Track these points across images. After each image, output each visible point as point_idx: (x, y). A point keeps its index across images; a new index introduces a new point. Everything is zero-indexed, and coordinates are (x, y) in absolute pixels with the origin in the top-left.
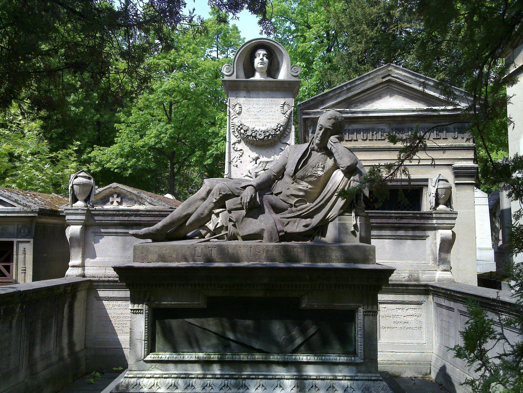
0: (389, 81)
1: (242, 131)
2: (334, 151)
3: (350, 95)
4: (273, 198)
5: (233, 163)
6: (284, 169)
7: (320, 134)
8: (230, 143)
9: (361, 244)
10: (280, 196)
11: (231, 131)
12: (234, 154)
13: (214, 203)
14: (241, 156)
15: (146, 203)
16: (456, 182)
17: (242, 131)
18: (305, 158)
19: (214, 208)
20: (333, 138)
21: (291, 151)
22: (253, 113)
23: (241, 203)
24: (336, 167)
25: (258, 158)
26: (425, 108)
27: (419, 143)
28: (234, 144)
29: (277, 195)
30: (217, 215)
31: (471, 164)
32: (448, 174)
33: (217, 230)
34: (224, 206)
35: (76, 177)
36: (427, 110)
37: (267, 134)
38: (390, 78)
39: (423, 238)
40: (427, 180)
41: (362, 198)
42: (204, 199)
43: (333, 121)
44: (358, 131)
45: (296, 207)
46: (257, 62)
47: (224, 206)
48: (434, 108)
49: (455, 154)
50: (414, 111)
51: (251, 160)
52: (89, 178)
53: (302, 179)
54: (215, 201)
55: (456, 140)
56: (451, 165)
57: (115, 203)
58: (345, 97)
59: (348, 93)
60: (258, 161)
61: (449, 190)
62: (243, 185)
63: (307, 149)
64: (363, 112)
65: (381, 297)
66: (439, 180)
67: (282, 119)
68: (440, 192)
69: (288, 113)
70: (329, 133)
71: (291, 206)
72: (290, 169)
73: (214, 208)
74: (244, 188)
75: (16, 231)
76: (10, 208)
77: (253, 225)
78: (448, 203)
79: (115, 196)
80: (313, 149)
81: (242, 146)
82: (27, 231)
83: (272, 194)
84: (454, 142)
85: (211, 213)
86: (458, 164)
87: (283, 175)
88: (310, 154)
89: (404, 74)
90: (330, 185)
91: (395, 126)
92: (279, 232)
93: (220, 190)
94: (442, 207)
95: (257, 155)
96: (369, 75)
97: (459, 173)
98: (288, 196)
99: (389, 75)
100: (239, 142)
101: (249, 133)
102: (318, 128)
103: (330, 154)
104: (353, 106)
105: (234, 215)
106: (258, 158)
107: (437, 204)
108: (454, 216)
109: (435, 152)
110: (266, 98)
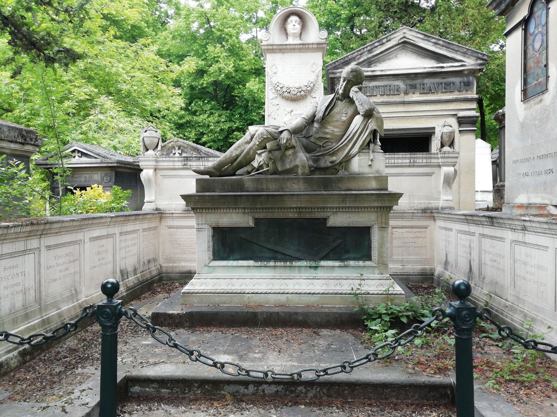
0: (405, 42)
1: (279, 88)
2: (355, 99)
3: (370, 56)
6: (314, 116)
7: (344, 85)
13: (258, 145)
16: (460, 129)
17: (279, 88)
18: (330, 107)
20: (355, 88)
21: (319, 101)
24: (356, 113)
25: (292, 111)
30: (260, 154)
32: (453, 122)
33: (260, 167)
37: (300, 90)
40: (434, 128)
41: (378, 137)
42: (248, 143)
45: (324, 147)
47: (265, 148)
50: (425, 68)
51: (286, 113)
54: (257, 143)
55: (461, 93)
56: (456, 115)
58: (365, 58)
60: (292, 114)
61: (452, 134)
62: (280, 130)
64: (382, 71)
65: (392, 223)
66: (445, 126)
68: (444, 136)
71: (320, 146)
74: (281, 132)
75: (100, 178)
76: (93, 160)
78: (452, 145)
79: (177, 148)
82: (108, 178)
84: (460, 95)
85: (255, 153)
86: (461, 114)
90: (352, 126)
91: (409, 82)
94: (446, 149)
95: (291, 109)
97: (462, 121)
101: (284, 90)
103: (352, 102)
104: (373, 65)
106: (292, 111)
107: (442, 146)
108: (456, 155)
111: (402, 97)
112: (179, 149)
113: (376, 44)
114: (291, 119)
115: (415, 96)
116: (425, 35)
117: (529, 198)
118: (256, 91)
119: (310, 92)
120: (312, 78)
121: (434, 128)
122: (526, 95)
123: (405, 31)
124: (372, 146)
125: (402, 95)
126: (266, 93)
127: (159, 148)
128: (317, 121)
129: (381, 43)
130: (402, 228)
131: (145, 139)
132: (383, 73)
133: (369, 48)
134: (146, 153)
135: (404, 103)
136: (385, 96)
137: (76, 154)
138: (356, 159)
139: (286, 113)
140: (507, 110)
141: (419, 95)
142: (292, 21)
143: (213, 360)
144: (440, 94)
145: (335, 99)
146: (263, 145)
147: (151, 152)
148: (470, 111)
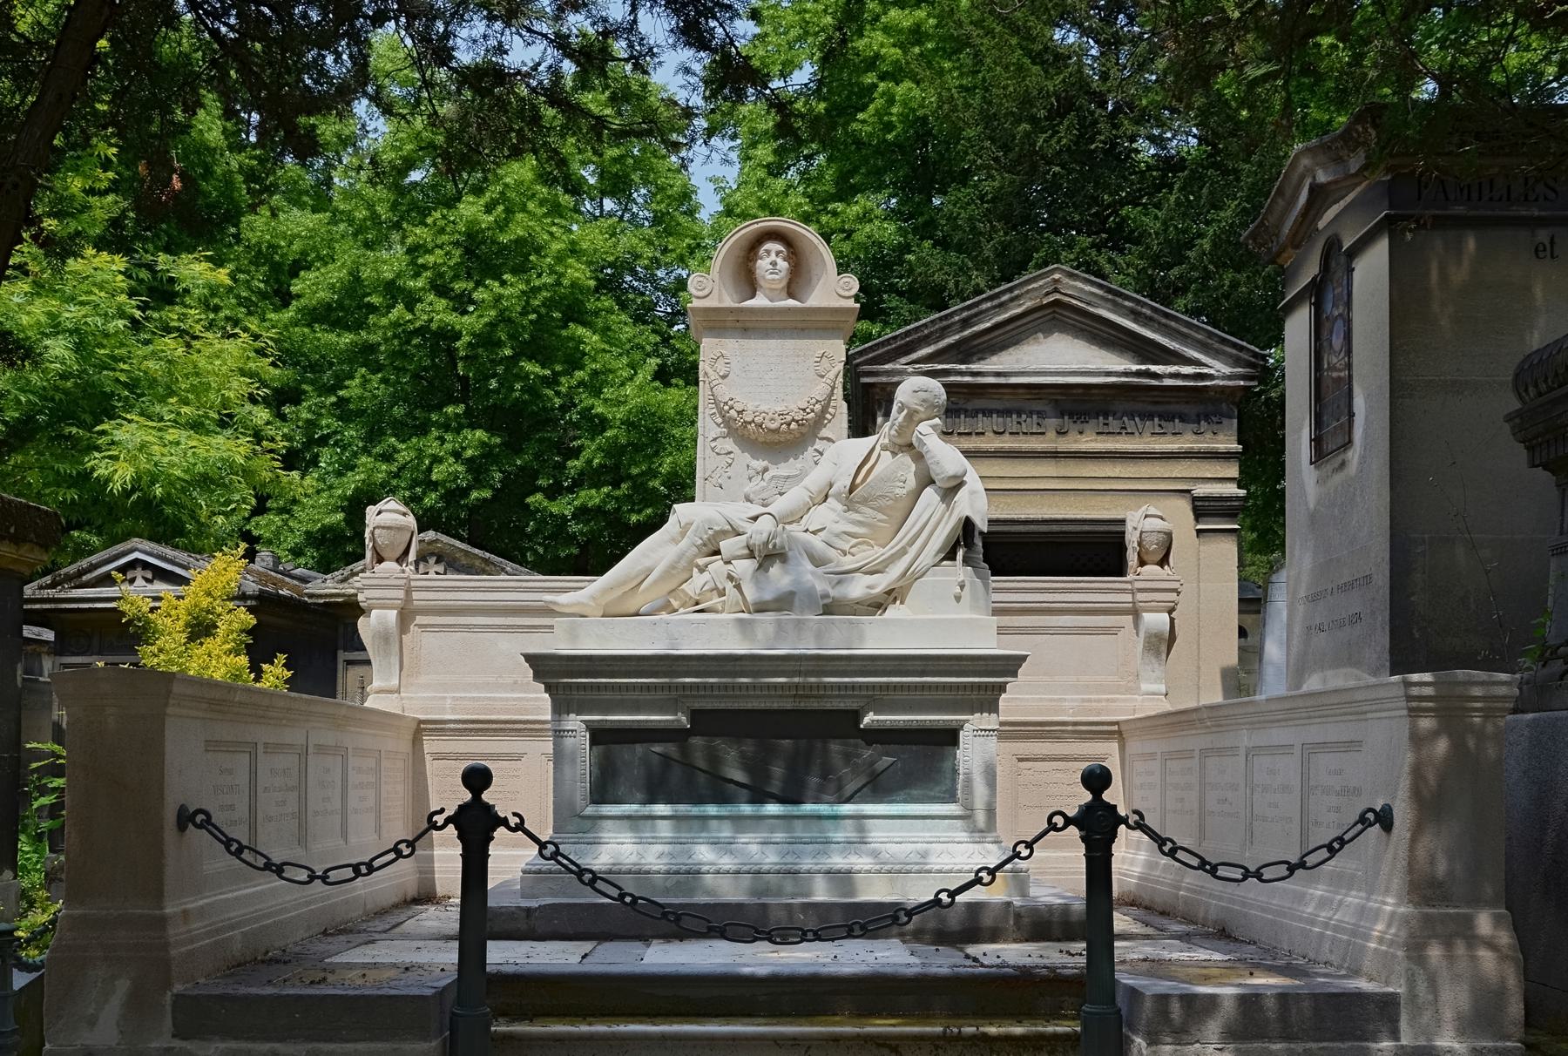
0: (1057, 303)
19: (696, 556)
26: (1135, 368)
27: (634, 273)
29: (814, 533)
31: (1232, 490)
32: (1184, 507)
34: (717, 552)
36: (1139, 374)
37: (789, 418)
38: (1058, 296)
40: (1123, 522)
44: (987, 413)
46: (763, 264)
47: (717, 552)
48: (1153, 368)
50: (1109, 374)
53: (865, 501)
55: (1200, 438)
56: (1188, 491)
59: (963, 329)
60: (767, 476)
64: (998, 374)
68: (1147, 539)
69: (831, 375)
70: (916, 419)
72: (830, 568)
73: (696, 556)
74: (755, 519)
79: (432, 560)
81: (729, 444)
86: (1201, 490)
89: (1088, 288)
96: (1011, 290)
98: (837, 535)
99: (1056, 290)
102: (895, 408)
106: (766, 470)
109: (1156, 463)
110: (785, 338)
111: (1052, 441)
112: (437, 562)
113: (984, 306)
115: (1084, 438)
116: (1109, 291)
117: (1324, 681)
118: (1058, 874)
119: (824, 410)
120: (819, 390)
121: (1123, 522)
122: (1320, 453)
123: (1057, 276)
125: (1051, 434)
126: (699, 424)
127: (412, 557)
128: (838, 497)
129: (996, 302)
130: (1043, 760)
131: (377, 532)
132: (1002, 380)
133: (965, 314)
134: (378, 568)
135: (1055, 455)
136: (1007, 436)
137: (139, 573)
139: (751, 472)
140: (1288, 484)
141: (1094, 437)
142: (768, 252)
143: (619, 888)
144: (1147, 438)
145: (878, 448)
147: (390, 565)
148: (1223, 482)
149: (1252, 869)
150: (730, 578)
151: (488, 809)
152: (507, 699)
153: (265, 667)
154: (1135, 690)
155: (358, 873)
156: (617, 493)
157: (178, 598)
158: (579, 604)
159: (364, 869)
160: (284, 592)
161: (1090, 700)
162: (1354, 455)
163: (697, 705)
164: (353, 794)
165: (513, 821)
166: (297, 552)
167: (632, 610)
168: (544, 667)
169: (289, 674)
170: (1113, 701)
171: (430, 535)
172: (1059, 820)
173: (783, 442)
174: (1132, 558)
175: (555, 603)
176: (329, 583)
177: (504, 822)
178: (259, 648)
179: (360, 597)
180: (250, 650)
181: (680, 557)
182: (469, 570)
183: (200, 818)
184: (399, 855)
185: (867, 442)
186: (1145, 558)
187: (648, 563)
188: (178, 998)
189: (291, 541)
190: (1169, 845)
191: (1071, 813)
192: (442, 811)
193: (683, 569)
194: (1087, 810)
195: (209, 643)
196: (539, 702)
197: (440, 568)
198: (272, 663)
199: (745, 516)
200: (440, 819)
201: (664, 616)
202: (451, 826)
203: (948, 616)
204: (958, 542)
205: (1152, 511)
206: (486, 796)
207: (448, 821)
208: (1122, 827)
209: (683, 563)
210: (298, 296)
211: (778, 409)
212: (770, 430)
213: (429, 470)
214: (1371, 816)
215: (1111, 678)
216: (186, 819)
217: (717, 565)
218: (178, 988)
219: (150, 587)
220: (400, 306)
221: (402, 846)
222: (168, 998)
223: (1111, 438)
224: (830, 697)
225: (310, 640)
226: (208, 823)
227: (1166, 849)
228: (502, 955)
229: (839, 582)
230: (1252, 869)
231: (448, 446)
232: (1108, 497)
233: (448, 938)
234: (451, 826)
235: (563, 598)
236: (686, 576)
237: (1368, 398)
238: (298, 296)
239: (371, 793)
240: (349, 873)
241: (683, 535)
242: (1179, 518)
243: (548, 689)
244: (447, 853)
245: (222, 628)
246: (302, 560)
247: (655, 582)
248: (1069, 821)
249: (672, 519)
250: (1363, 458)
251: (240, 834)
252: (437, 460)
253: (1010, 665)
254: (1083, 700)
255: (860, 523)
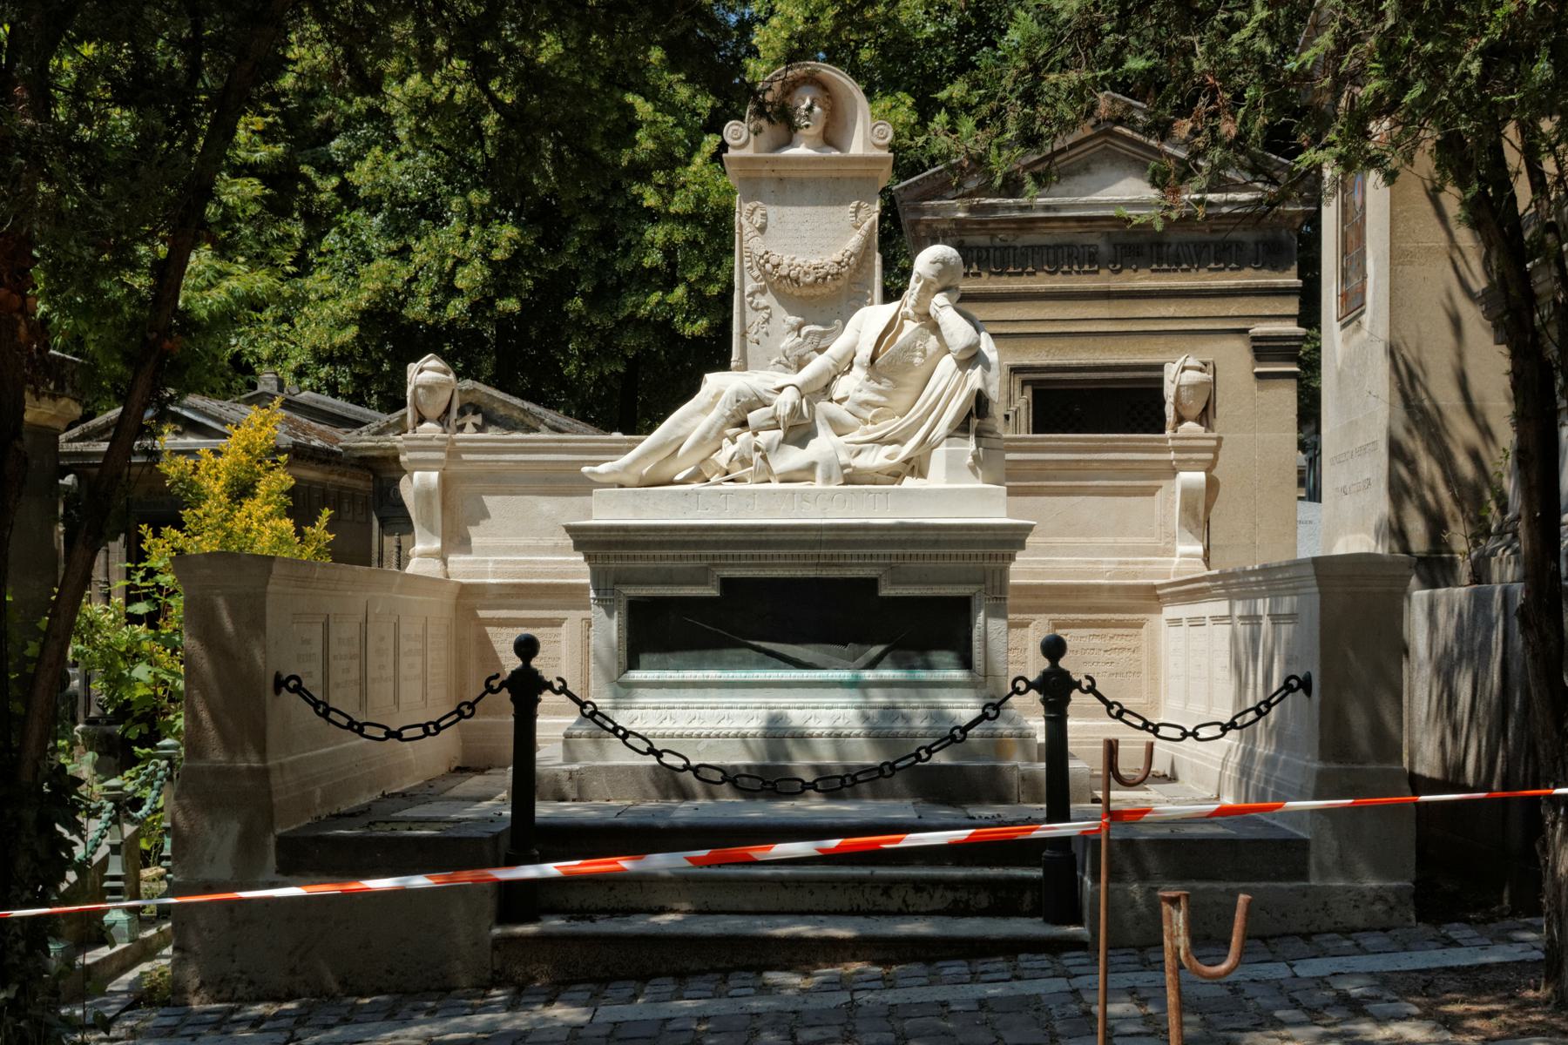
4: (833, 408)
5: (751, 336)
8: (742, 291)
9: (1506, 794)
10: (845, 404)
11: (746, 265)
12: (751, 316)
14: (767, 321)
15: (541, 427)
17: (768, 266)
22: (790, 226)
23: (773, 418)
28: (752, 294)
29: (839, 401)
34: (744, 424)
35: (421, 371)
39: (1150, 492)
43: (939, 266)
47: (744, 424)
49: (1016, 350)
52: (445, 372)
56: (1245, 331)
57: (469, 427)
60: (804, 331)
63: (895, 318)
64: (1047, 208)
67: (854, 241)
68: (1184, 393)
69: (866, 226)
72: (865, 352)
74: (780, 390)
77: (794, 457)
78: (1205, 416)
80: (906, 317)
83: (831, 400)
86: (1260, 329)
87: (851, 362)
88: (902, 325)
92: (844, 467)
93: (738, 393)
100: (763, 291)
105: (764, 437)
114: (800, 345)
115: (1138, 275)
121: (1160, 367)
124: (975, 422)
127: (454, 414)
128: (861, 365)
131: (420, 390)
135: (1108, 295)
138: (943, 448)
146: (739, 418)
149: (1190, 730)
150: (757, 449)
151: (1065, 675)
152: (548, 562)
153: (308, 529)
154: (1169, 552)
155: (427, 733)
156: (671, 299)
157: (217, 453)
158: (615, 472)
159: (432, 729)
160: (316, 443)
161: (1127, 563)
162: (1366, 318)
163: (726, 573)
164: (404, 662)
165: (557, 685)
166: (300, 373)
167: (666, 477)
168: (587, 540)
169: (331, 537)
170: (1150, 563)
171: (468, 384)
172: (1021, 685)
173: (823, 300)
174: (1169, 410)
175: (594, 473)
176: (365, 436)
177: (549, 686)
178: (300, 506)
179: (402, 458)
180: (290, 513)
181: (710, 429)
182: (509, 425)
183: (292, 683)
184: (436, 724)
185: (895, 305)
186: (1183, 413)
187: (681, 432)
188: (281, 841)
189: (297, 358)
190: (1116, 708)
191: (1031, 679)
192: (497, 676)
193: (712, 440)
194: (1046, 675)
195: (249, 505)
196: (576, 569)
197: (478, 419)
198: (313, 526)
199: (771, 387)
200: (495, 684)
201: (696, 486)
202: (505, 690)
203: (954, 494)
204: (970, 414)
205: (1191, 362)
206: (535, 663)
207: (503, 685)
208: (1076, 691)
209: (713, 433)
210: (295, 62)
211: (815, 261)
212: (806, 285)
213: (452, 273)
214: (1294, 682)
215: (1148, 540)
216: (280, 684)
217: (745, 436)
218: (279, 831)
219: (180, 440)
220: (418, 77)
221: (464, 708)
222: (272, 840)
223: (1166, 275)
224: (851, 565)
225: (356, 503)
226: (299, 689)
227: (1114, 712)
228: (544, 810)
229: (859, 452)
230: (1190, 730)
231: (473, 245)
232: (1162, 339)
233: (545, 741)
234: (505, 690)
235: (602, 468)
236: (715, 446)
237: (1376, 260)
238: (295, 62)
239: (418, 660)
240: (419, 731)
241: (712, 405)
242: (1235, 358)
243: (588, 558)
244: (500, 717)
245: (262, 489)
246: (306, 382)
247: (688, 452)
248: (1030, 686)
249: (704, 388)
250: (1372, 321)
251: (319, 696)
252: (459, 262)
253: (1011, 539)
254: (1120, 563)
255: (880, 392)
